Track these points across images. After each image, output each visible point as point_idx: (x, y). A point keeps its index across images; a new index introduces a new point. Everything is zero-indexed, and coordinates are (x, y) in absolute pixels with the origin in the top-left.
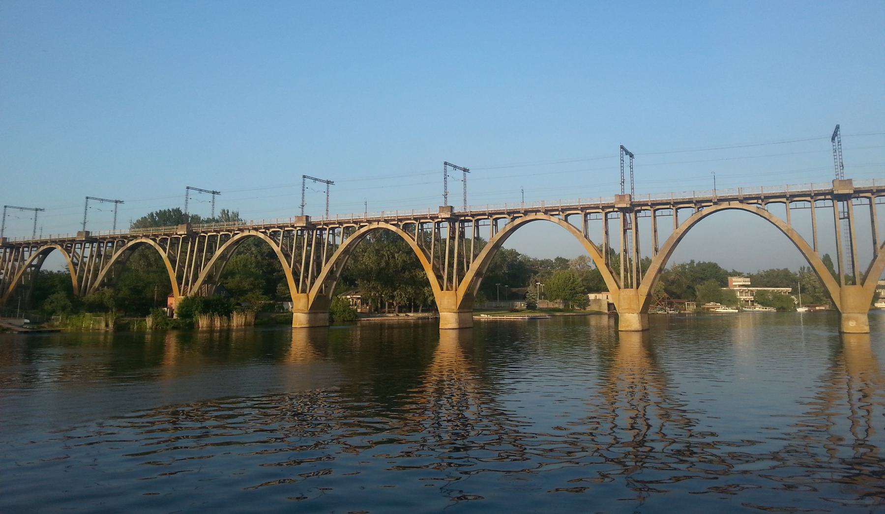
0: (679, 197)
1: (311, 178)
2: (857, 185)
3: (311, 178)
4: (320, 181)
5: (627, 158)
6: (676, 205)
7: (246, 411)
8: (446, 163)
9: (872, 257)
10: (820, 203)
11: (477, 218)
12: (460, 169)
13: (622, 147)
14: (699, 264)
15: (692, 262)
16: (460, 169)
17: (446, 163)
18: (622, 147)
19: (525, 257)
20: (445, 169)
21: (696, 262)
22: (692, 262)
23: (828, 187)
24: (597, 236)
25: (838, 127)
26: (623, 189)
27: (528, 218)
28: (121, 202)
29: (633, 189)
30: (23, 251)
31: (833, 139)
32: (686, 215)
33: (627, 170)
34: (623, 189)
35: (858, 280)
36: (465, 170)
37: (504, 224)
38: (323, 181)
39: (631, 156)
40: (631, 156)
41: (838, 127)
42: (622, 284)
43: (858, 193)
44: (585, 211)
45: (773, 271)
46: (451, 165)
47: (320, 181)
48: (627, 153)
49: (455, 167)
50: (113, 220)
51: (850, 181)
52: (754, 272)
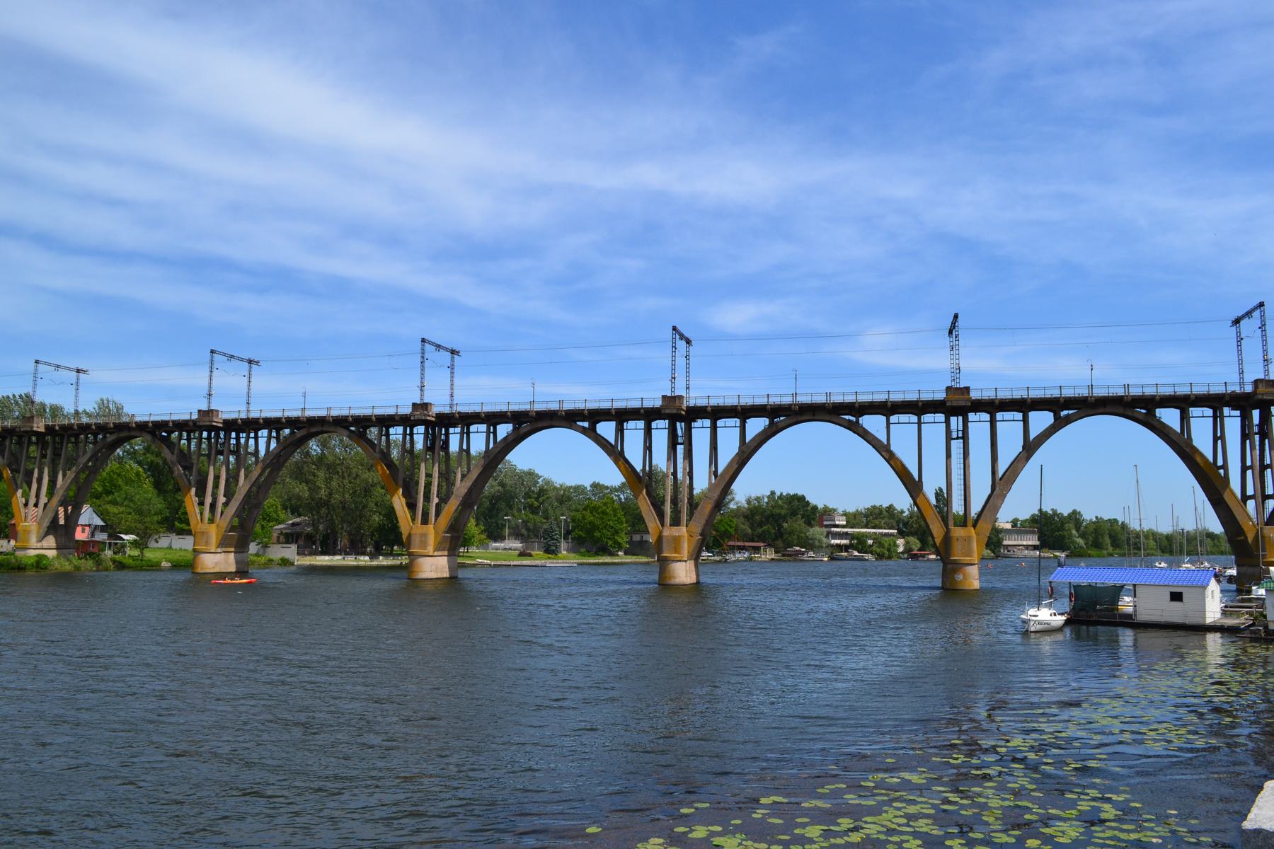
0: (746, 401)
1: (225, 354)
2: (974, 395)
3: (225, 354)
4: (238, 359)
5: (681, 345)
6: (1024, 406)
7: (833, 737)
8: (423, 341)
9: (989, 491)
10: (927, 417)
11: (467, 420)
12: (446, 349)
13: (674, 329)
14: (781, 497)
15: (773, 493)
16: (446, 349)
17: (423, 341)
18: (674, 329)
19: (548, 482)
20: (1249, 314)
21: (778, 494)
22: (773, 493)
23: (941, 395)
24: (634, 454)
25: (956, 316)
26: (673, 388)
27: (313, 430)
28: (85, 372)
29: (688, 388)
30: (447, 434)
31: (951, 332)
32: (756, 425)
33: (680, 361)
34: (673, 388)
35: (970, 523)
36: (453, 352)
37: (504, 430)
38: (243, 360)
39: (688, 342)
40: (688, 342)
41: (956, 316)
42: (668, 520)
43: (979, 406)
44: (621, 416)
45: (874, 507)
46: (432, 343)
47: (238, 359)
48: (682, 337)
49: (438, 346)
50: (246, 390)
51: (967, 389)
52: (851, 510)
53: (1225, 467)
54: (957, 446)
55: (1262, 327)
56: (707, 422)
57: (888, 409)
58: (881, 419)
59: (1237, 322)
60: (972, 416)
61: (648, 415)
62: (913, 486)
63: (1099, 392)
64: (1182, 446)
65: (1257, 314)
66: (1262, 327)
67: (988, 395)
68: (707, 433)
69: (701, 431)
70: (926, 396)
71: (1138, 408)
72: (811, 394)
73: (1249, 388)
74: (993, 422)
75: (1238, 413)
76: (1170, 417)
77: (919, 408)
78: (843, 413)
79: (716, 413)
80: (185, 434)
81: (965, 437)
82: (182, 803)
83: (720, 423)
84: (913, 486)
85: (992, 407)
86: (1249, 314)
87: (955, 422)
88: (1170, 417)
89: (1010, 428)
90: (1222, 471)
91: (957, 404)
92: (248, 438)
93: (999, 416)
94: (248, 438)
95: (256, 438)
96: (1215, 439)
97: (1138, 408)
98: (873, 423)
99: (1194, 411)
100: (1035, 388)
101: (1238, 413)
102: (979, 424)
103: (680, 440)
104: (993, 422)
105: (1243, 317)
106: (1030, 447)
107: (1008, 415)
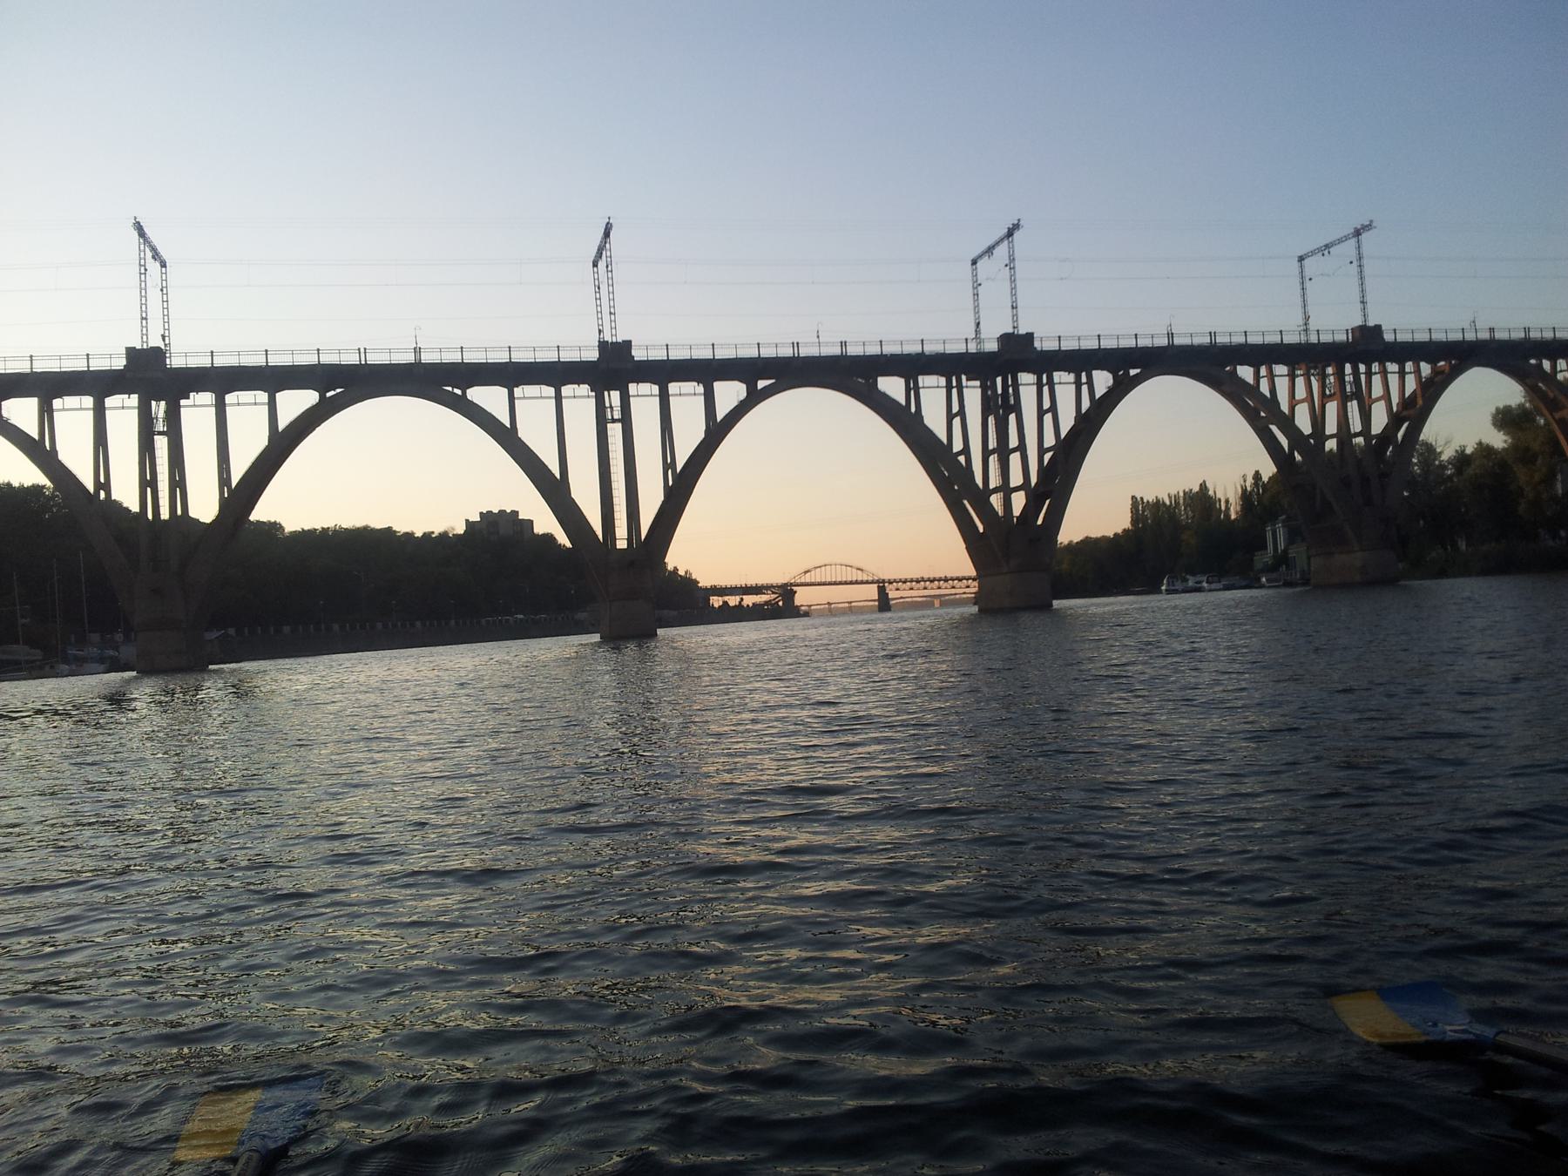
2: (638, 354)
5: (154, 267)
26: (145, 334)
34: (145, 334)
37: (1103, 380)
39: (163, 265)
53: (966, 450)
54: (615, 432)
55: (1011, 264)
56: (207, 398)
57: (511, 375)
58: (500, 393)
59: (1301, 259)
60: (632, 388)
61: (98, 385)
62: (554, 489)
63: (677, 354)
64: (906, 422)
65: (1002, 251)
66: (1011, 264)
67: (658, 355)
68: (132, 418)
69: (197, 412)
70: (568, 356)
71: (850, 374)
72: (389, 348)
73: (992, 346)
74: (221, 408)
75: (978, 383)
76: (892, 386)
77: (556, 374)
78: (438, 382)
79: (223, 380)
80: (1362, 368)
81: (626, 421)
82: (101, 1024)
83: (230, 398)
84: (554, 489)
85: (664, 373)
86: (990, 250)
87: (159, 409)
88: (892, 386)
89: (687, 401)
90: (962, 459)
91: (613, 369)
92: (1369, 374)
93: (673, 387)
94: (1369, 374)
95: (1384, 373)
96: (950, 417)
97: (850, 374)
98: (491, 398)
99: (924, 380)
100: (931, 341)
101: (978, 383)
102: (644, 398)
103: (160, 426)
104: (221, 408)
105: (980, 256)
106: (716, 432)
107: (71, 401)
